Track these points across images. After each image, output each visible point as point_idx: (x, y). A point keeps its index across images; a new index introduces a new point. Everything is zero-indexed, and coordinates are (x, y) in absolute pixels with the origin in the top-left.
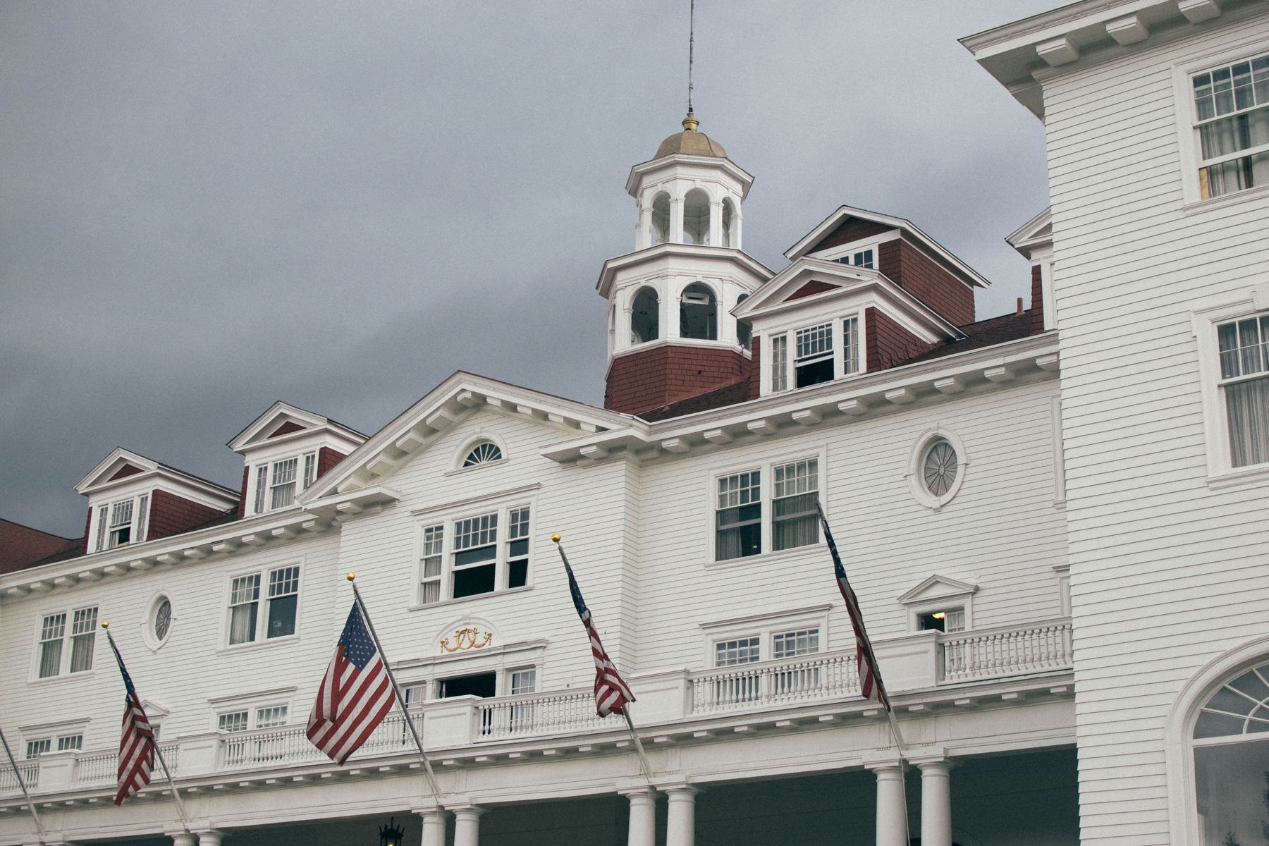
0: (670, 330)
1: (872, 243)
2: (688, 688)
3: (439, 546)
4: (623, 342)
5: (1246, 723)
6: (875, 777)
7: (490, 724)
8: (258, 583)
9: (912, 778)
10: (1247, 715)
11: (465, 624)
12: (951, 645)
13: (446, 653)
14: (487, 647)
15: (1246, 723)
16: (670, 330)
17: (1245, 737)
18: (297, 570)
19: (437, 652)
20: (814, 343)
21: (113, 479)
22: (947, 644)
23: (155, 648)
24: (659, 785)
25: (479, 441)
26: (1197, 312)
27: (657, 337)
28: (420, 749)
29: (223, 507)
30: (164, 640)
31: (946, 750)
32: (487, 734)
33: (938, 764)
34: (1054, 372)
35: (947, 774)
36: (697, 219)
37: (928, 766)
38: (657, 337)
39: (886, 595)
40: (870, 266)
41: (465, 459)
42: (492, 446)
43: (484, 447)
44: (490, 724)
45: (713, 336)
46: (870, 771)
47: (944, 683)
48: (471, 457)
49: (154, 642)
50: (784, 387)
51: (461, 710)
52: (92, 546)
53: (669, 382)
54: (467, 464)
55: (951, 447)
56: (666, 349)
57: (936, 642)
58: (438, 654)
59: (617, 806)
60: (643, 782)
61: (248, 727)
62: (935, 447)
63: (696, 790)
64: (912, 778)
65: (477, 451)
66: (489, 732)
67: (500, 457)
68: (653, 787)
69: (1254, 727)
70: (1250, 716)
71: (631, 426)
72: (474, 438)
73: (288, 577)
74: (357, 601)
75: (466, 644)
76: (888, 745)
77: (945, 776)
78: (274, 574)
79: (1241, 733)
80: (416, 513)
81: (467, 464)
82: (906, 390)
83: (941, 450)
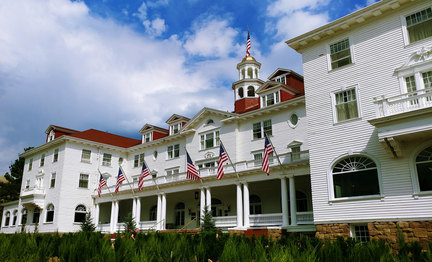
0: (246, 95)
1: (284, 75)
2: (291, 156)
3: (203, 139)
4: (238, 98)
5: (342, 170)
6: (281, 180)
7: (273, 162)
8: (172, 147)
9: (287, 180)
10: (430, 157)
11: (208, 153)
12: (294, 155)
13: (205, 159)
14: (213, 157)
15: (342, 170)
16: (246, 95)
17: (366, 169)
18: (179, 145)
19: (204, 159)
20: (270, 97)
21: (170, 121)
22: (293, 155)
23: (155, 160)
24: (205, 187)
25: (209, 119)
26: (331, 92)
27: (243, 97)
28: (236, 171)
29: (166, 133)
30: (156, 158)
31: (293, 175)
32: (272, 164)
33: (292, 177)
34: (304, 104)
35: (210, 189)
36: (250, 73)
37: (291, 178)
38: (243, 97)
39: (163, 169)
40: (280, 82)
41: (207, 123)
42: (212, 120)
43: (210, 121)
44: (273, 162)
45: (254, 96)
46: (280, 179)
47: (292, 162)
48: (208, 123)
49: (154, 158)
50: (279, 102)
51: (288, 155)
52: (143, 142)
53: (246, 105)
54: (208, 124)
55: (297, 116)
56: (245, 99)
57: (291, 154)
58: (204, 159)
59: (278, 181)
60: (202, 187)
61: (107, 184)
62: (294, 116)
63: (248, 183)
64: (287, 180)
65: (209, 121)
66: (273, 164)
67: (213, 122)
68: (241, 183)
69: (344, 171)
70: (343, 169)
71: (236, 116)
72: (208, 119)
73: (178, 146)
74: (120, 167)
75: (209, 157)
76: (283, 174)
77: (292, 180)
78: (175, 146)
79: (341, 171)
80: (199, 134)
81: (208, 124)
82: (296, 104)
83: (295, 117)
